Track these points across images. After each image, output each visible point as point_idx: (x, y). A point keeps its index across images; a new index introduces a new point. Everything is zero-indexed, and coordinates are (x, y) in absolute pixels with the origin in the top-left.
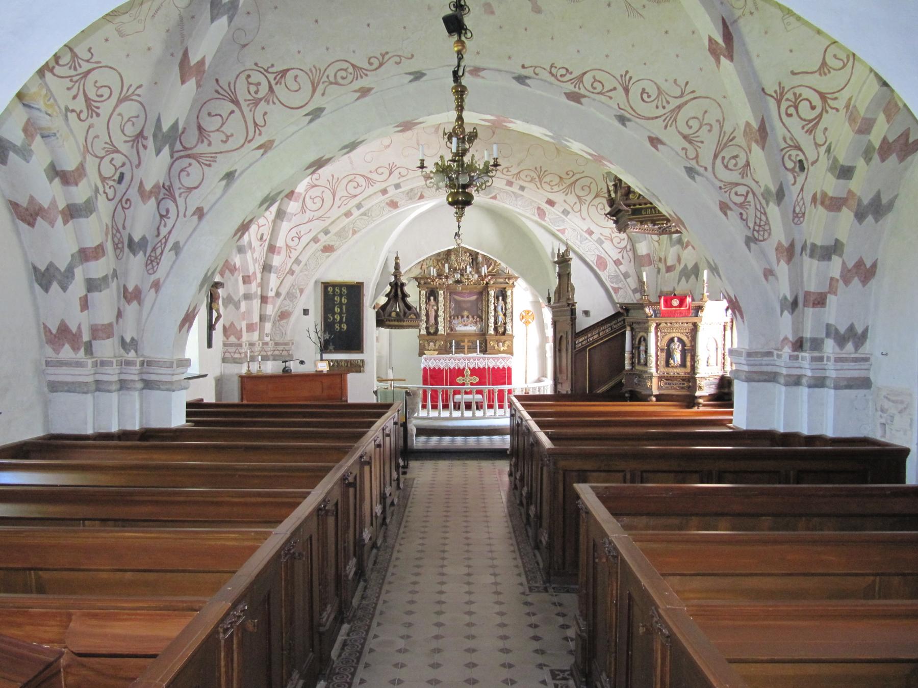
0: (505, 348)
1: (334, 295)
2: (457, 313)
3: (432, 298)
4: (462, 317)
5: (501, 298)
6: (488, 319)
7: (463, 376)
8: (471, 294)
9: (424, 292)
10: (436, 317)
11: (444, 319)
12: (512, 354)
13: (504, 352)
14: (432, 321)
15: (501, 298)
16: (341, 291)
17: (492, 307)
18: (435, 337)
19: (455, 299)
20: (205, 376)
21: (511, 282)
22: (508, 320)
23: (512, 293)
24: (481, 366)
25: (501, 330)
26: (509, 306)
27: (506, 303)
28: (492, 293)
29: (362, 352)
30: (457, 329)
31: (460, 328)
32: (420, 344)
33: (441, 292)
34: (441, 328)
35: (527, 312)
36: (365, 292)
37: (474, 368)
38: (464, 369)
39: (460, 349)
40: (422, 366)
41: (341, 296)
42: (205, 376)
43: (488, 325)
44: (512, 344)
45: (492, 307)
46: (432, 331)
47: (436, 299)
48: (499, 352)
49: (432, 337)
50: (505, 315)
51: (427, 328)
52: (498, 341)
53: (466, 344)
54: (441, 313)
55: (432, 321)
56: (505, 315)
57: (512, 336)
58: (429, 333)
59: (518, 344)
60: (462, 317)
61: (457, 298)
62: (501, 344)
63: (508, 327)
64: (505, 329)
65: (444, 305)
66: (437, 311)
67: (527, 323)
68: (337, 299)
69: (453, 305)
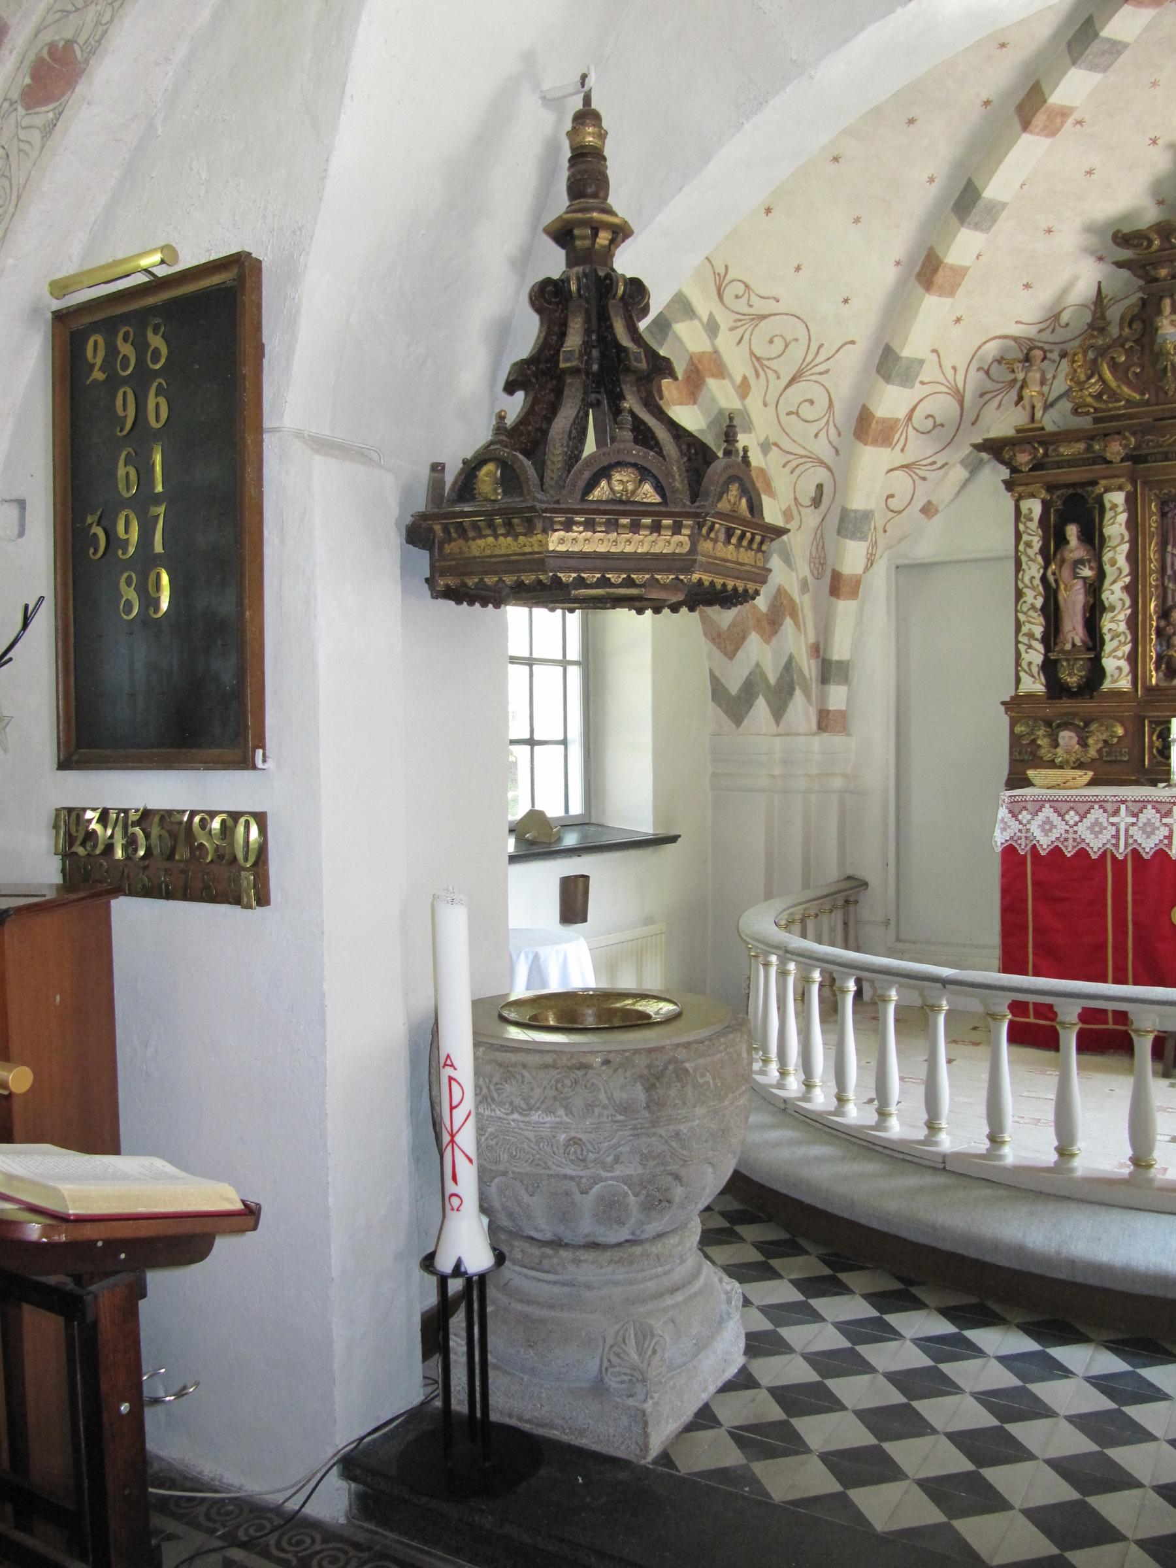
1: (113, 382)
3: (1072, 531)
9: (1034, 507)
10: (1095, 610)
11: (1132, 622)
14: (1074, 631)
16: (141, 346)
18: (1084, 706)
20: (673, 839)
29: (246, 763)
32: (1015, 739)
34: (1115, 662)
36: (272, 338)
40: (1000, 838)
41: (141, 380)
42: (673, 839)
46: (1072, 678)
47: (1094, 539)
49: (1065, 705)
51: (1049, 667)
54: (1114, 593)
55: (1074, 631)
58: (1056, 688)
65: (1132, 557)
66: (1095, 588)
68: (125, 406)
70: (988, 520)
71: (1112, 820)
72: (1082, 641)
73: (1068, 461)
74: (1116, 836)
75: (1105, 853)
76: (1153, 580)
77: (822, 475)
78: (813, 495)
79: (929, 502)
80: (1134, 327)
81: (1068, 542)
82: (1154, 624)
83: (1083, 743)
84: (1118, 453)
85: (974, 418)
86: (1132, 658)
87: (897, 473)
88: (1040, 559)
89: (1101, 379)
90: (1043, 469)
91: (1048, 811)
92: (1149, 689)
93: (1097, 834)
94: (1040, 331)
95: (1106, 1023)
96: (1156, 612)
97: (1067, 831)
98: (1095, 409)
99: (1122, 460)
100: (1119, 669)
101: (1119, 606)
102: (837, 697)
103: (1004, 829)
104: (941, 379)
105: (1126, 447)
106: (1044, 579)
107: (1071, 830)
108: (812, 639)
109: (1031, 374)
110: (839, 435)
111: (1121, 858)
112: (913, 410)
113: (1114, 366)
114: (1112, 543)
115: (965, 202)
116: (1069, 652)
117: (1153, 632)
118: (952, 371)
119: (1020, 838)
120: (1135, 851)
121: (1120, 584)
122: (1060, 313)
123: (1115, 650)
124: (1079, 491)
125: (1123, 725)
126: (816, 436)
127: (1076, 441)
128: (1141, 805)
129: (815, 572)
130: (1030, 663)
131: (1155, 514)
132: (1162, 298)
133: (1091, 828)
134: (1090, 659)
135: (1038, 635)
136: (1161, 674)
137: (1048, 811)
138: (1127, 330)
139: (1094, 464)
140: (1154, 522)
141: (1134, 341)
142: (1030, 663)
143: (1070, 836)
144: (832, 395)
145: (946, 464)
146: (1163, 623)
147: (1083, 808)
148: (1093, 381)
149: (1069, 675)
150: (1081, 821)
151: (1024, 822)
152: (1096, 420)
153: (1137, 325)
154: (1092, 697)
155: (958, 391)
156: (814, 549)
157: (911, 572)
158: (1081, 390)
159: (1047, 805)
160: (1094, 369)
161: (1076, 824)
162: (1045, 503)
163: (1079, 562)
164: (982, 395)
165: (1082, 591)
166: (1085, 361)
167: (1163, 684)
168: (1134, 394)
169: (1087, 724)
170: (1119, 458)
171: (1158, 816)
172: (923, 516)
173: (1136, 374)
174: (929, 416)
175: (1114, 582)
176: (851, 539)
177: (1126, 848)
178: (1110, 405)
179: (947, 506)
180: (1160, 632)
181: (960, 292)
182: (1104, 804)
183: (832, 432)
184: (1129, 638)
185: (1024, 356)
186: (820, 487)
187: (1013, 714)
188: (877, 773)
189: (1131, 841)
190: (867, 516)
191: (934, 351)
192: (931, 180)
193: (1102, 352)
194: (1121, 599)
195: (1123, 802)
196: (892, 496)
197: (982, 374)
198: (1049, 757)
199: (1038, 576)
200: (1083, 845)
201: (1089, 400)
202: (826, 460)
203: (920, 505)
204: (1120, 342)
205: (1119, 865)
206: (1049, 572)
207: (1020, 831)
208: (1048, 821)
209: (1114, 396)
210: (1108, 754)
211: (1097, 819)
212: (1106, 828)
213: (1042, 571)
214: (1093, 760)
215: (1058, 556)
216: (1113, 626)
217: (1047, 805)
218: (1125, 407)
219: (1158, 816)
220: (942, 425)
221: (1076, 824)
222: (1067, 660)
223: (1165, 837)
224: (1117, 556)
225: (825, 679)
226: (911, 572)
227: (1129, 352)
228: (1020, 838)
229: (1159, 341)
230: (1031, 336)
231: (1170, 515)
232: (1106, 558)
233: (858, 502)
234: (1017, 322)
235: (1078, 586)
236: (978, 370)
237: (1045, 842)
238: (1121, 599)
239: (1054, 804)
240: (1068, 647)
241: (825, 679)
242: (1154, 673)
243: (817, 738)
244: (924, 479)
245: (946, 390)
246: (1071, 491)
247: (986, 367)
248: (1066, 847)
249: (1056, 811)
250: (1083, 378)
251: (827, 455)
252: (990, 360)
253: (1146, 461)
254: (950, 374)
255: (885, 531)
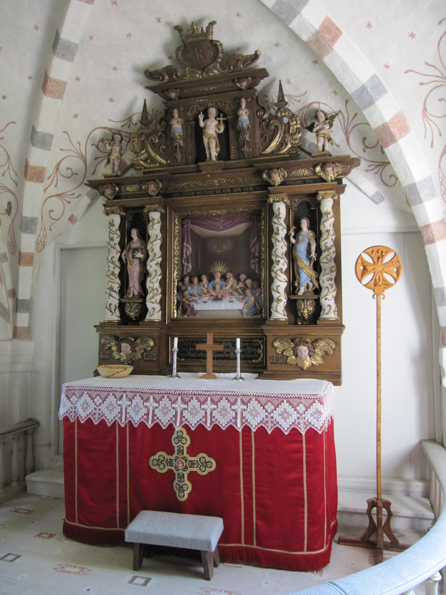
0: (318, 360)
2: (202, 265)
4: (211, 278)
5: (305, 224)
6: (271, 280)
7: (170, 451)
8: (232, 219)
9: (117, 219)
12: (335, 378)
13: (314, 373)
15: (305, 224)
17: (281, 248)
19: (193, 234)
21: (331, 173)
22: (326, 280)
23: (336, 205)
24: (223, 423)
25: (307, 309)
26: (327, 241)
27: (318, 235)
28: (281, 208)
30: (198, 307)
31: (205, 306)
32: (102, 346)
33: (155, 216)
34: (153, 305)
35: (378, 253)
37: (201, 427)
38: (171, 428)
39: (192, 360)
40: (62, 412)
43: (271, 299)
44: (337, 350)
45: (281, 248)
46: (132, 313)
47: (144, 237)
48: (300, 372)
50: (317, 267)
51: (122, 306)
52: (296, 341)
53: (209, 347)
54: (153, 266)
55: (134, 287)
56: (317, 267)
57: (338, 326)
58: (125, 319)
59: (355, 347)
60: (211, 278)
61: (199, 230)
62: (304, 350)
63: (328, 300)
64: (318, 308)
65: (163, 248)
66: (143, 263)
67: (378, 287)
69: (189, 250)
70: (100, 227)
71: (119, 402)
72: (139, 293)
73: (132, 195)
74: (121, 413)
75: (115, 421)
76: (176, 260)
77: (9, 197)
78: (6, 208)
79: (72, 215)
80: (162, 124)
81: (133, 239)
82: (176, 284)
83: (133, 350)
84: (153, 191)
85: (93, 171)
86: (163, 302)
87: (53, 198)
88: (118, 247)
89: (147, 151)
90: (120, 199)
91: (86, 397)
92: (173, 320)
93: (110, 411)
94: (122, 126)
95: (116, 527)
96: (177, 278)
97: (95, 409)
98: (145, 167)
99: (157, 195)
100: (154, 309)
101: (154, 274)
102: (23, 319)
103: (64, 407)
104: (72, 148)
105: (157, 188)
106: (120, 259)
107: (97, 408)
108: (9, 287)
109: (114, 147)
110: (16, 175)
111: (123, 426)
112: (59, 164)
113: (153, 145)
114: (151, 240)
115: (53, 43)
116: (130, 299)
117: (175, 289)
118: (78, 145)
119: (71, 412)
120: (130, 422)
121: (155, 262)
122: (131, 117)
123: (152, 298)
124: (140, 211)
125: (154, 340)
126: (3, 175)
127: (134, 184)
128: (134, 394)
129: (11, 251)
130: (110, 304)
131: (177, 225)
132: (174, 109)
133: (107, 407)
134: (141, 303)
135: (117, 290)
136: (179, 312)
137: (86, 397)
138: (159, 126)
139: (145, 197)
140: (177, 229)
141: (162, 132)
142: (110, 304)
143: (97, 412)
144: (9, 152)
145: (80, 195)
146: (180, 284)
147: (104, 395)
148: (143, 152)
149: (130, 311)
150: (103, 403)
151: (74, 402)
152: (144, 173)
153: (163, 123)
154: (139, 325)
155: (83, 156)
156: (9, 238)
157: (68, 253)
158: (137, 157)
159: (85, 393)
160: (143, 146)
161: (100, 405)
162: (122, 218)
163: (135, 250)
164: (96, 159)
165: (138, 265)
166: (138, 141)
167: (180, 317)
168: (163, 161)
169: (135, 340)
170: (155, 194)
171: (142, 401)
172: (70, 223)
173: (164, 150)
174: (68, 169)
175: (152, 261)
176: (25, 232)
177: (126, 420)
178: (151, 166)
179: (82, 217)
180: (179, 289)
181: (65, 96)
182: (115, 393)
183: (12, 173)
184: (160, 291)
185: (112, 137)
186: (9, 203)
187: (100, 333)
188: (47, 360)
189: (128, 416)
190: (33, 221)
191: (65, 132)
192: (37, 28)
193: (148, 136)
194: (155, 271)
195: (125, 392)
196: (52, 211)
197: (94, 147)
198: (117, 357)
199: (117, 256)
200: (103, 418)
201: (142, 162)
202: (12, 190)
203: (68, 217)
204: (155, 132)
205: (122, 430)
206: (123, 254)
207: (71, 408)
208: (86, 402)
209: (154, 161)
210: (147, 356)
211: (111, 402)
212: (115, 408)
213: (119, 254)
214: (139, 360)
215: (128, 246)
216: (151, 285)
217: (85, 393)
218: (158, 167)
219: (142, 401)
220: (76, 174)
221: (100, 405)
222: (129, 303)
223: (145, 414)
224: (155, 246)
225: (16, 309)
226: (68, 253)
227: (160, 137)
228: (71, 412)
229: (172, 132)
230: (118, 129)
231: (185, 226)
232: (149, 247)
233: (27, 213)
234: (109, 120)
235: (136, 262)
236: (92, 145)
237: (83, 415)
238: (155, 271)
239: (88, 392)
240: (131, 296)
241: (16, 309)
242: (175, 311)
243: (10, 342)
244: (69, 202)
245: (76, 155)
246: (136, 212)
247: (96, 144)
248: (95, 419)
249: (90, 396)
250: (138, 151)
251: (11, 186)
252: (98, 140)
253: (172, 197)
254: (77, 146)
255: (51, 230)
